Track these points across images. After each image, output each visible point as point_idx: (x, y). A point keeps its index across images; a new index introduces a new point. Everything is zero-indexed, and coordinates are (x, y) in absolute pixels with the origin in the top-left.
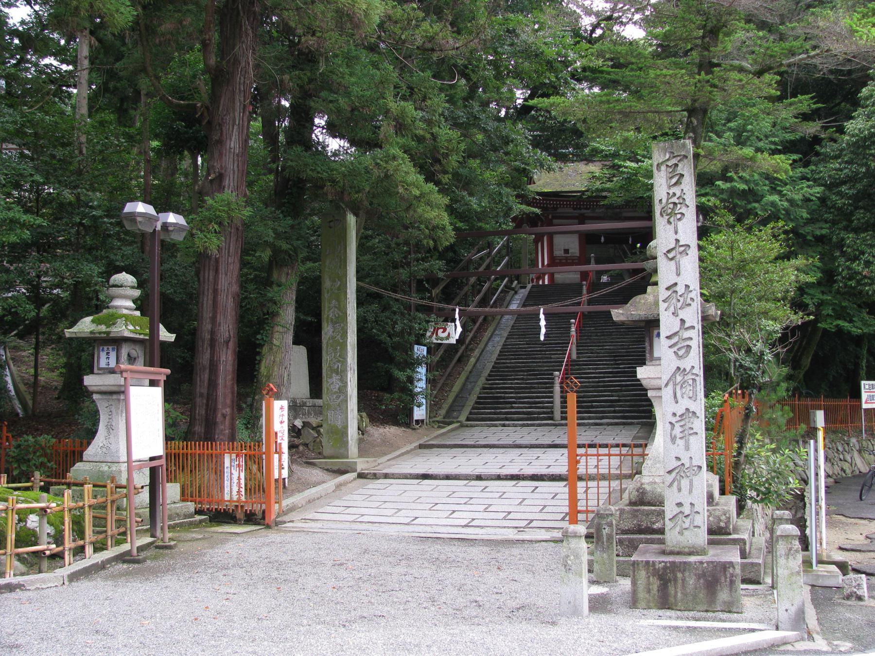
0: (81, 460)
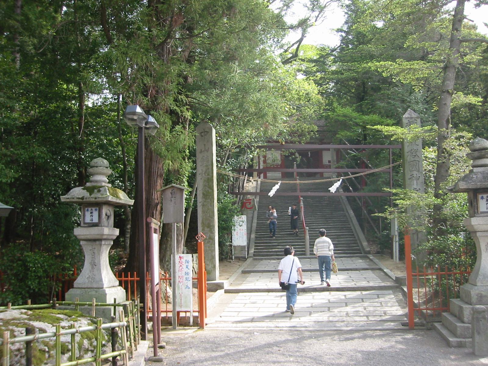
0: (73, 287)
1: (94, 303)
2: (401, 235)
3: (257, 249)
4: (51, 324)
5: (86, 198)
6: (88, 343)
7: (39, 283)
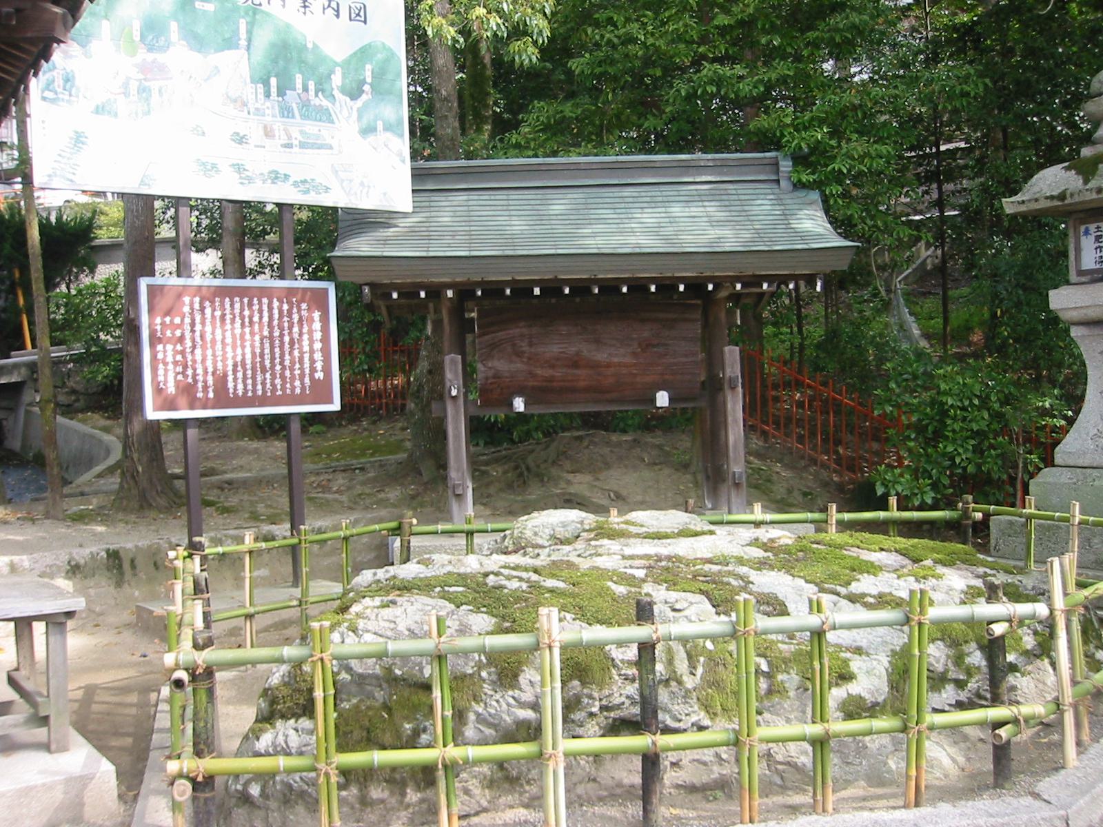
1: (1074, 516)
2: (426, 775)
3: (418, 204)
4: (817, 584)
5: (1072, 195)
6: (948, 656)
7: (978, 450)
